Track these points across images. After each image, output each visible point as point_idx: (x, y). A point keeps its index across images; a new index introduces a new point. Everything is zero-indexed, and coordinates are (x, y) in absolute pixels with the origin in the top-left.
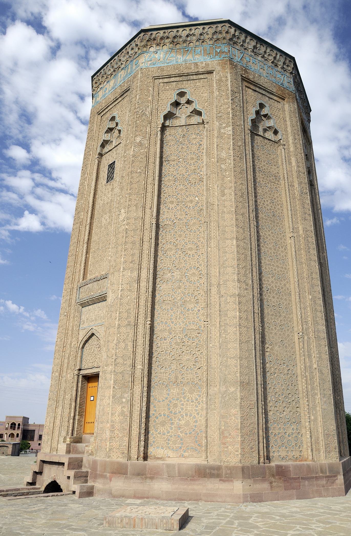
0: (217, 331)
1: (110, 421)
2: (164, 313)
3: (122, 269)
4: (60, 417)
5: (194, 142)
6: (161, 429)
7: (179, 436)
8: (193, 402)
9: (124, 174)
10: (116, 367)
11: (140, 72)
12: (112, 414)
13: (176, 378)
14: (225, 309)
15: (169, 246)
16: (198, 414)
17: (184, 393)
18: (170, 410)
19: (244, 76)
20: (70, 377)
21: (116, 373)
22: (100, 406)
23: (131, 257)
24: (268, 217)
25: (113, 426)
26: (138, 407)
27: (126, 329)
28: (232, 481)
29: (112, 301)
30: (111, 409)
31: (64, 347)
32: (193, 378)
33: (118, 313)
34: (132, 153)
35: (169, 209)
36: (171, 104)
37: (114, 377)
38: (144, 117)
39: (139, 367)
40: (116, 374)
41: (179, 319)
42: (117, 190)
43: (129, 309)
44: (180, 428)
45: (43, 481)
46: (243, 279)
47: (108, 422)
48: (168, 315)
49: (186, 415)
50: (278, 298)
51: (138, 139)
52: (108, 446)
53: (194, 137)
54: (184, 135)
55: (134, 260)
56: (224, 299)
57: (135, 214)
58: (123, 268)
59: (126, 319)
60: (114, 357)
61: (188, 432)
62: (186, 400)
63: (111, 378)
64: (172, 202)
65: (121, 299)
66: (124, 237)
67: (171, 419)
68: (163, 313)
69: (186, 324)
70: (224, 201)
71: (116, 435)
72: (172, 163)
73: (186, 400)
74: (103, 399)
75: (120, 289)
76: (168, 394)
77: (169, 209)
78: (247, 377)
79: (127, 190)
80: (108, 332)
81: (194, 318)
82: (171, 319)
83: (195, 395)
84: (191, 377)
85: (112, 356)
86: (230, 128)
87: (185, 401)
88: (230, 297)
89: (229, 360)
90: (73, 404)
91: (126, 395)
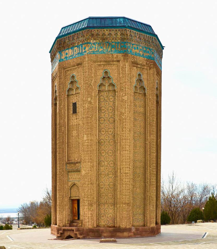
6: (102, 218)
13: (107, 201)
15: (102, 151)
21: (88, 201)
49: (110, 213)
51: (89, 99)
60: (87, 195)
64: (103, 131)
67: (105, 215)
70: (123, 134)
77: (102, 134)
90: (69, 210)
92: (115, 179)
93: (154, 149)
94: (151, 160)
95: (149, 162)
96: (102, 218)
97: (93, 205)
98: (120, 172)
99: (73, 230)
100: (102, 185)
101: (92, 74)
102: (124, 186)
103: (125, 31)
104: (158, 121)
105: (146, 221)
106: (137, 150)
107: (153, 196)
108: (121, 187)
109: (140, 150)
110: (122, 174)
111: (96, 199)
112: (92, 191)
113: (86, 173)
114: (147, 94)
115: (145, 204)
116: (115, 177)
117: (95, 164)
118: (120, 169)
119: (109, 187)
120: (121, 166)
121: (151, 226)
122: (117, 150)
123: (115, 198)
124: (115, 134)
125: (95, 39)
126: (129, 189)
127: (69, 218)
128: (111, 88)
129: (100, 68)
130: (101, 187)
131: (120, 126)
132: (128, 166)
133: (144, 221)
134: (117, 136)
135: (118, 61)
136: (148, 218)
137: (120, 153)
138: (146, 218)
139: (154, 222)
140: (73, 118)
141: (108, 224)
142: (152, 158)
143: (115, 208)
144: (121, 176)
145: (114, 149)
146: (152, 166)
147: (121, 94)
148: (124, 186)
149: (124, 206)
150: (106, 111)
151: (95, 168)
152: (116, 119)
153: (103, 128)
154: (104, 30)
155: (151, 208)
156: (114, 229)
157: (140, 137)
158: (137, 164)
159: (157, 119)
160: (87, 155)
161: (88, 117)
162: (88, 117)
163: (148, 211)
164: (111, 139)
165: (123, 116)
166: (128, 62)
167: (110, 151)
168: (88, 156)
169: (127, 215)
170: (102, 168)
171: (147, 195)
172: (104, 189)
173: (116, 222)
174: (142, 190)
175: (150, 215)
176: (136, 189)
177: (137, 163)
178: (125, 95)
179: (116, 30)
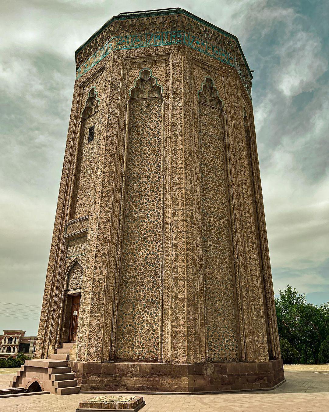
0: (170, 259)
2: (131, 245)
6: (128, 337)
7: (141, 342)
8: (151, 315)
9: (101, 137)
14: (176, 242)
16: (156, 324)
17: (145, 308)
18: (135, 322)
19: (195, 57)
20: (58, 296)
26: (110, 320)
29: (92, 237)
31: (54, 273)
32: (152, 296)
33: (96, 246)
38: (116, 91)
40: (93, 294)
43: (105, 243)
44: (141, 336)
46: (190, 219)
48: (134, 246)
50: (218, 233)
54: (147, 106)
55: (109, 205)
56: (175, 234)
57: (109, 169)
58: (100, 211)
59: (102, 251)
62: (146, 313)
64: (138, 160)
67: (135, 329)
69: (147, 254)
71: (93, 342)
72: (138, 129)
73: (146, 313)
75: (98, 227)
77: (135, 165)
78: (192, 295)
83: (153, 310)
86: (182, 101)
87: (146, 315)
89: (178, 281)
91: (101, 311)
93: (248, 198)
94: (244, 216)
95: (238, 219)
96: (128, 337)
100: (130, 259)
103: (179, 17)
104: (254, 166)
105: (243, 348)
107: (255, 290)
109: (216, 195)
111: (114, 290)
115: (238, 307)
121: (258, 361)
125: (127, 31)
126: (193, 268)
130: (128, 263)
133: (239, 347)
136: (248, 341)
139: (264, 352)
150: (144, 128)
153: (139, 155)
155: (255, 315)
157: (216, 174)
159: (249, 149)
164: (152, 172)
165: (176, 130)
166: (185, 55)
167: (150, 193)
169: (188, 328)
170: (131, 225)
172: (135, 269)
174: (227, 274)
176: (211, 270)
177: (212, 219)
179: (163, 18)
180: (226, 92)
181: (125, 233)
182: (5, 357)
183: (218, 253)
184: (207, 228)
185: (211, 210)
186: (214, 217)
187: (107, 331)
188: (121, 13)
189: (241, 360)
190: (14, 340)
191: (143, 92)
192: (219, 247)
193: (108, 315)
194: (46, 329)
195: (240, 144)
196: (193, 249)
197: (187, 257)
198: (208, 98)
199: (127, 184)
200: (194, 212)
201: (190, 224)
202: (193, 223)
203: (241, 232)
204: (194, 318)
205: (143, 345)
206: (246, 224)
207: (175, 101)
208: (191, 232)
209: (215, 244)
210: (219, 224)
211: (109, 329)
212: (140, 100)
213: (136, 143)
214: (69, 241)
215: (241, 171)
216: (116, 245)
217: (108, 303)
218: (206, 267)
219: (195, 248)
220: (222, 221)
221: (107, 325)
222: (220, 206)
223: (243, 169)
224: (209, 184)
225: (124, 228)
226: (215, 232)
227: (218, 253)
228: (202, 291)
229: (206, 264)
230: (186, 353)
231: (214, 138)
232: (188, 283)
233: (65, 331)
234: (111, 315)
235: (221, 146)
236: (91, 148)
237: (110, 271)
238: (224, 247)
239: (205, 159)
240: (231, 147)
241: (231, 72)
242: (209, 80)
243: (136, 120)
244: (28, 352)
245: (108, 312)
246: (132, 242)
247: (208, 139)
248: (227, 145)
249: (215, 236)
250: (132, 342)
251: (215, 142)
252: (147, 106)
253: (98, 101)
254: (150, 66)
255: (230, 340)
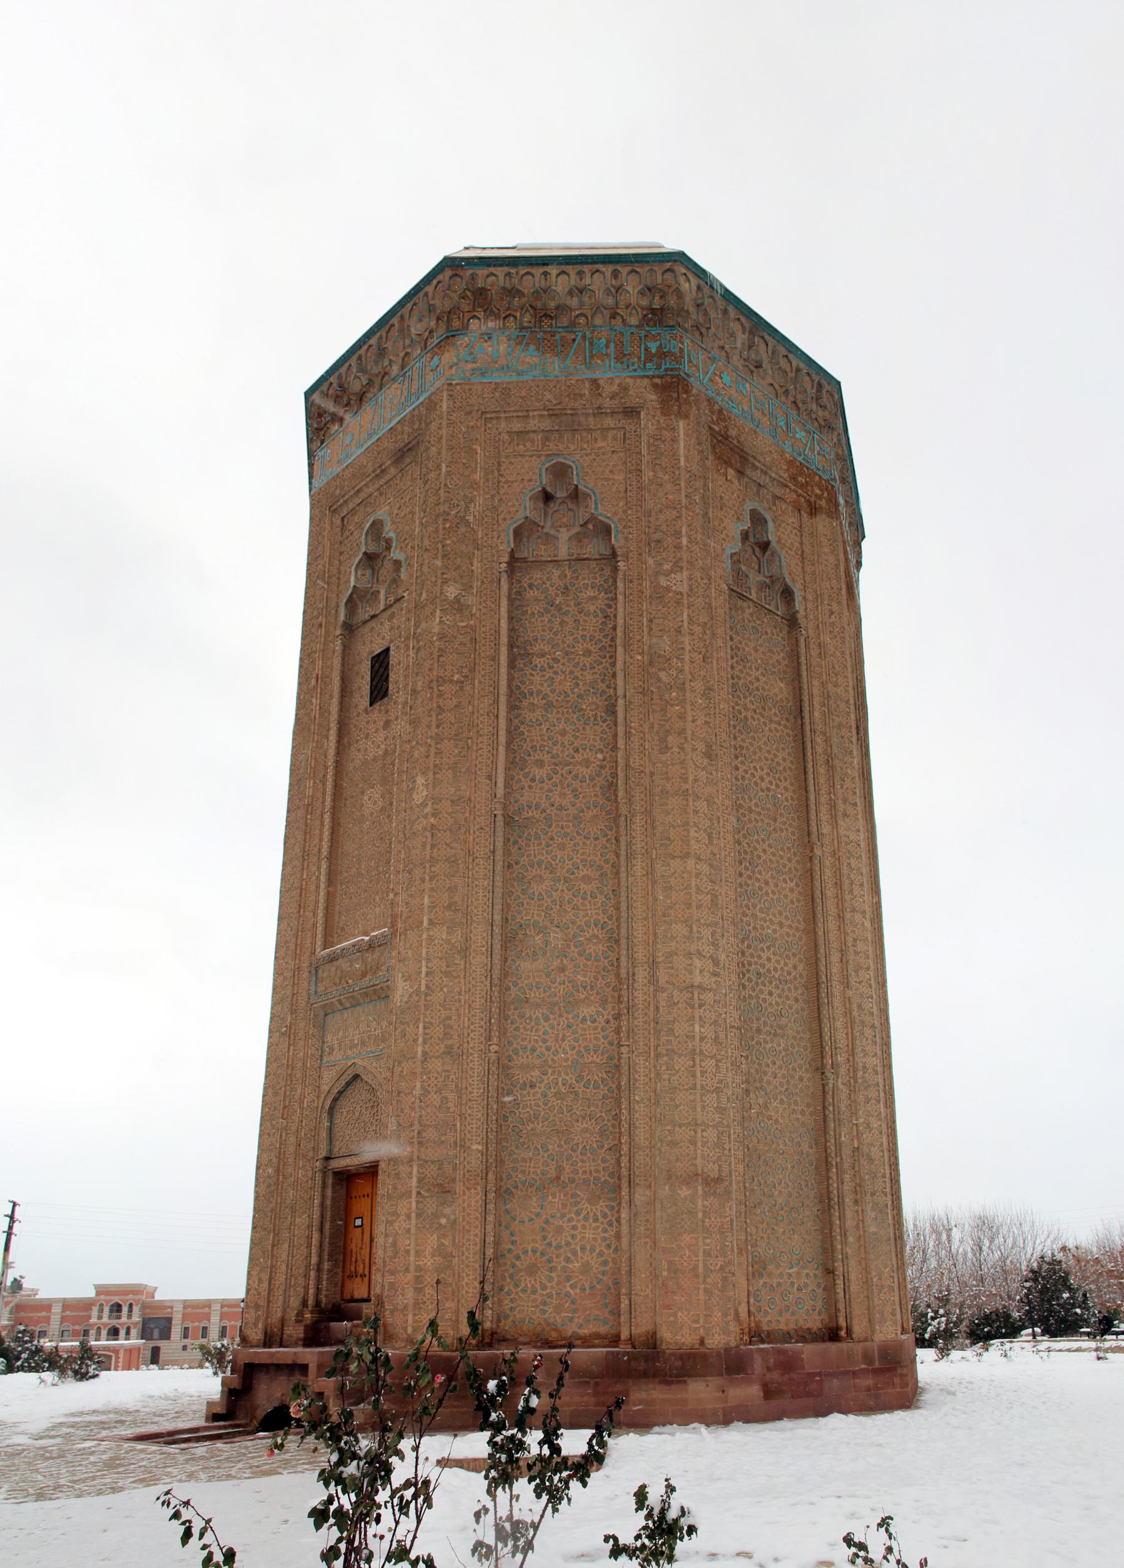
1: (412, 1268)
2: (529, 1027)
3: (425, 924)
4: (284, 1267)
5: (592, 608)
6: (528, 1281)
7: (567, 1294)
8: (596, 1220)
9: (420, 684)
10: (422, 1150)
11: (445, 394)
12: (417, 1252)
13: (560, 1169)
20: (305, 1174)
22: (386, 1235)
23: (446, 894)
24: (763, 809)
25: (418, 1279)
26: (476, 1235)
27: (444, 1064)
28: (685, 1382)
29: (406, 999)
30: (413, 1240)
31: (285, 1107)
33: (421, 1025)
34: (436, 630)
35: (533, 780)
36: (530, 498)
37: (418, 1172)
38: (463, 530)
39: (475, 1147)
41: (563, 1040)
42: (401, 727)
45: (254, 1408)
47: (407, 1270)
48: (537, 1030)
49: (583, 1249)
51: (452, 591)
52: (410, 1321)
53: (592, 594)
54: (566, 588)
56: (665, 994)
58: (430, 920)
61: (587, 1286)
62: (581, 1217)
63: (411, 1173)
64: (540, 763)
65: (426, 995)
66: (428, 847)
67: (550, 1261)
68: (524, 1028)
72: (537, 661)
73: (581, 1217)
74: (392, 1222)
76: (542, 1207)
77: (533, 780)
79: (429, 727)
80: (397, 1070)
81: (596, 1039)
82: (545, 1041)
84: (592, 1168)
85: (412, 1125)
87: (579, 1221)
88: (681, 991)
90: (316, 1236)
92: (618, 1031)
95: (835, 958)
97: (459, 1187)
98: (653, 979)
99: (304, 1368)
101: (474, 471)
102: (682, 1063)
103: (668, 275)
105: (841, 1306)
106: (758, 880)
108: (658, 1074)
110: (663, 990)
111: (485, 1153)
112: (452, 1096)
113: (418, 992)
114: (802, 622)
116: (618, 1017)
117: (479, 935)
118: (653, 964)
119: (580, 1078)
120: (655, 942)
121: (879, 1337)
122: (630, 856)
123: (616, 1149)
124: (615, 775)
126: (717, 1090)
127: (311, 1291)
128: (593, 548)
129: (521, 447)
130: (521, 1077)
131: (646, 726)
132: (708, 950)
134: (627, 778)
135: (631, 412)
137: (650, 872)
138: (840, 1282)
140: (372, 728)
141: (571, 1319)
142: (855, 940)
143: (618, 1211)
144: (657, 1008)
145: (611, 856)
146: (860, 983)
147: (650, 561)
148: (682, 1063)
149: (684, 1192)
151: (478, 961)
152: (620, 692)
154: (545, 274)
156: (607, 1352)
157: (775, 820)
158: (763, 960)
160: (427, 885)
161: (440, 681)
162: (440, 681)
163: (851, 1239)
165: (665, 670)
168: (432, 889)
169: (707, 1254)
170: (526, 965)
171: (839, 1146)
173: (624, 1303)
175: (867, 1270)
178: (677, 567)
180: (807, 562)
181: (508, 989)
182: (109, 1350)
183: (780, 1052)
184: (749, 980)
185: (763, 928)
186: (769, 948)
187: (468, 1266)
188: (467, 248)
189: (832, 1334)
190: (125, 1309)
191: (549, 539)
192: (783, 1036)
193: (468, 1223)
194: (272, 1267)
195: (844, 731)
196: (717, 1038)
197: (701, 1060)
198: (755, 579)
199: (509, 840)
200: (719, 931)
201: (709, 966)
202: (716, 963)
203: (843, 993)
204: (722, 1227)
205: (573, 1303)
206: (856, 972)
207: (657, 574)
208: (710, 990)
209: (771, 1027)
210: (782, 969)
211: (476, 1262)
212: (541, 563)
213: (533, 707)
214: (326, 1015)
215: (845, 815)
216: (483, 1023)
217: (469, 1189)
218: (747, 1091)
219: (722, 1036)
220: (791, 963)
221: (467, 1249)
222: (787, 918)
223: (850, 811)
224: (756, 849)
225: (505, 974)
226: (771, 994)
227: (780, 1052)
228: (740, 1154)
229: (747, 1082)
230: (701, 1321)
231: (770, 709)
232: (705, 1134)
233: (329, 1271)
234: (477, 1223)
235: (788, 734)
236: (382, 723)
237: (470, 1100)
238: (794, 1038)
239: (746, 771)
240: (819, 739)
241: (819, 497)
242: (757, 519)
243: (533, 631)
244: (168, 1338)
245: (469, 1214)
246: (530, 1018)
247: (755, 711)
248: (808, 733)
249: (770, 1004)
250: (542, 1295)
251: (771, 721)
252: (566, 588)
253: (397, 564)
254: (572, 447)
255: (806, 1285)
